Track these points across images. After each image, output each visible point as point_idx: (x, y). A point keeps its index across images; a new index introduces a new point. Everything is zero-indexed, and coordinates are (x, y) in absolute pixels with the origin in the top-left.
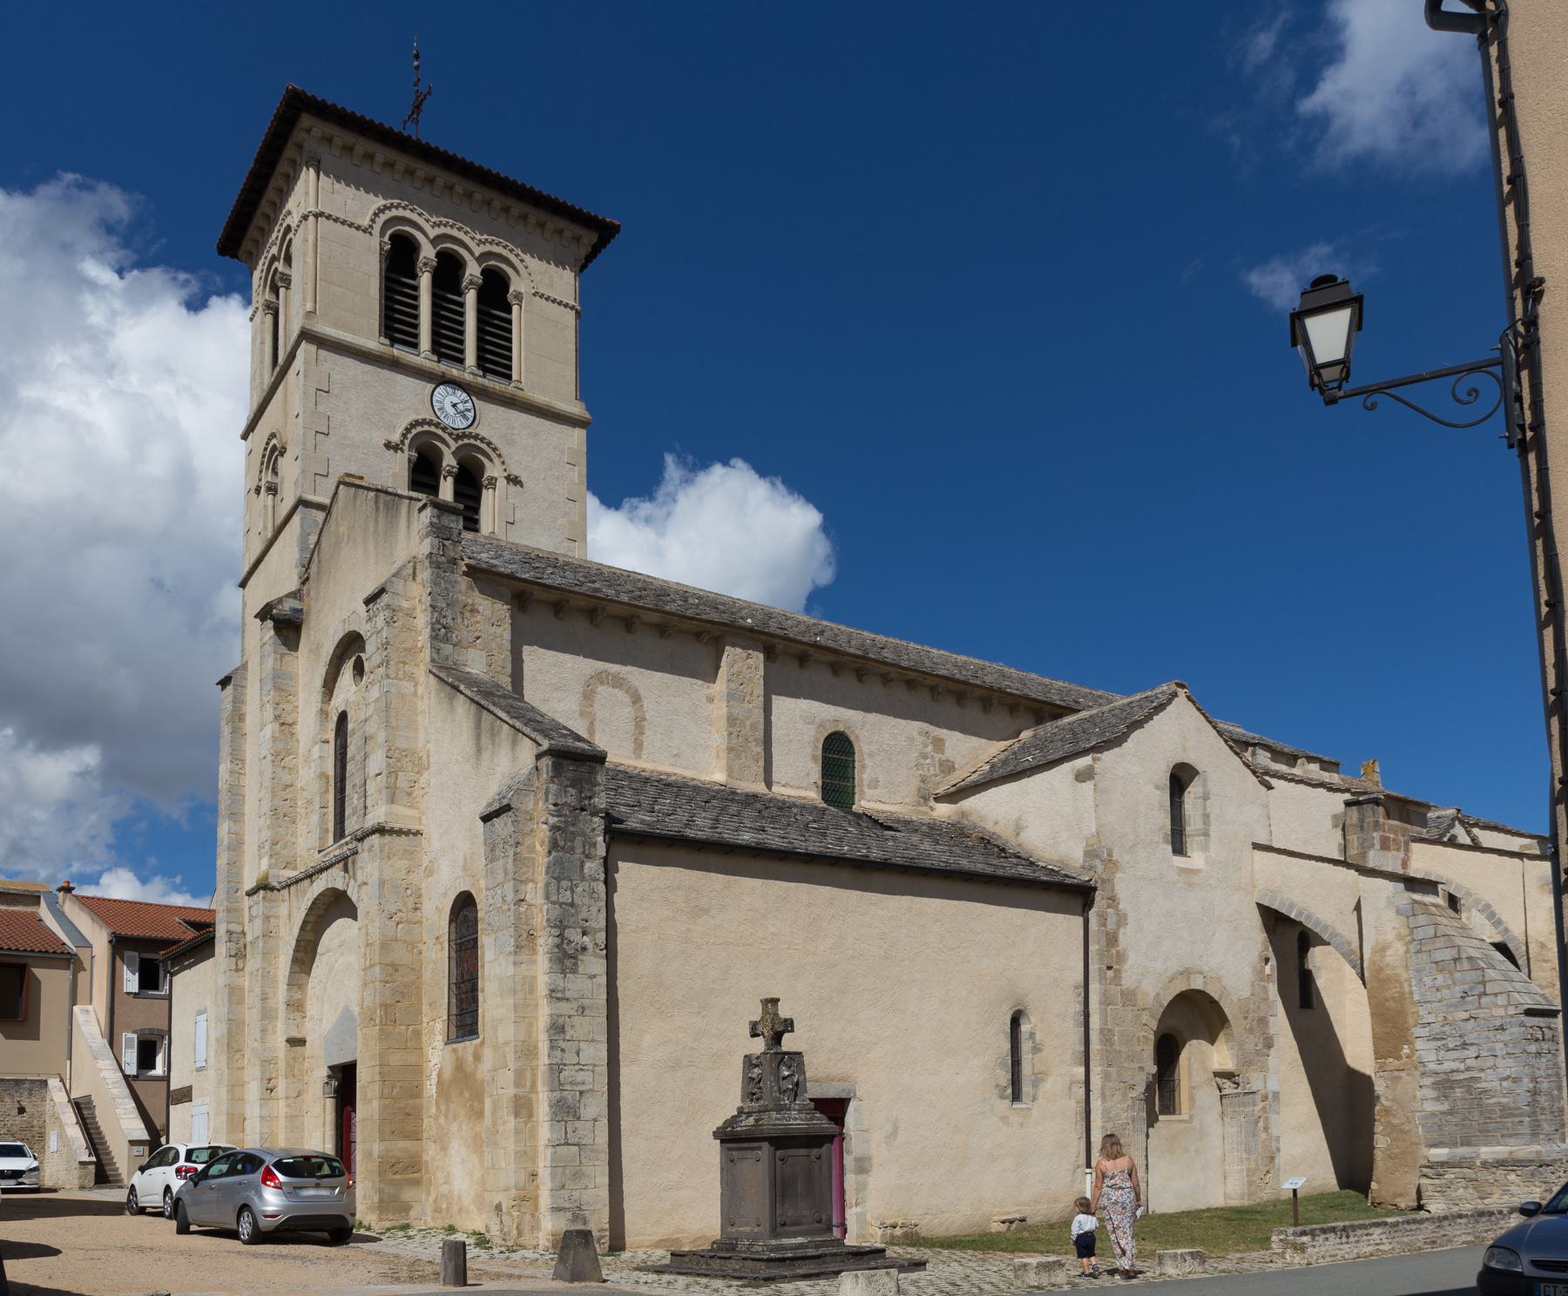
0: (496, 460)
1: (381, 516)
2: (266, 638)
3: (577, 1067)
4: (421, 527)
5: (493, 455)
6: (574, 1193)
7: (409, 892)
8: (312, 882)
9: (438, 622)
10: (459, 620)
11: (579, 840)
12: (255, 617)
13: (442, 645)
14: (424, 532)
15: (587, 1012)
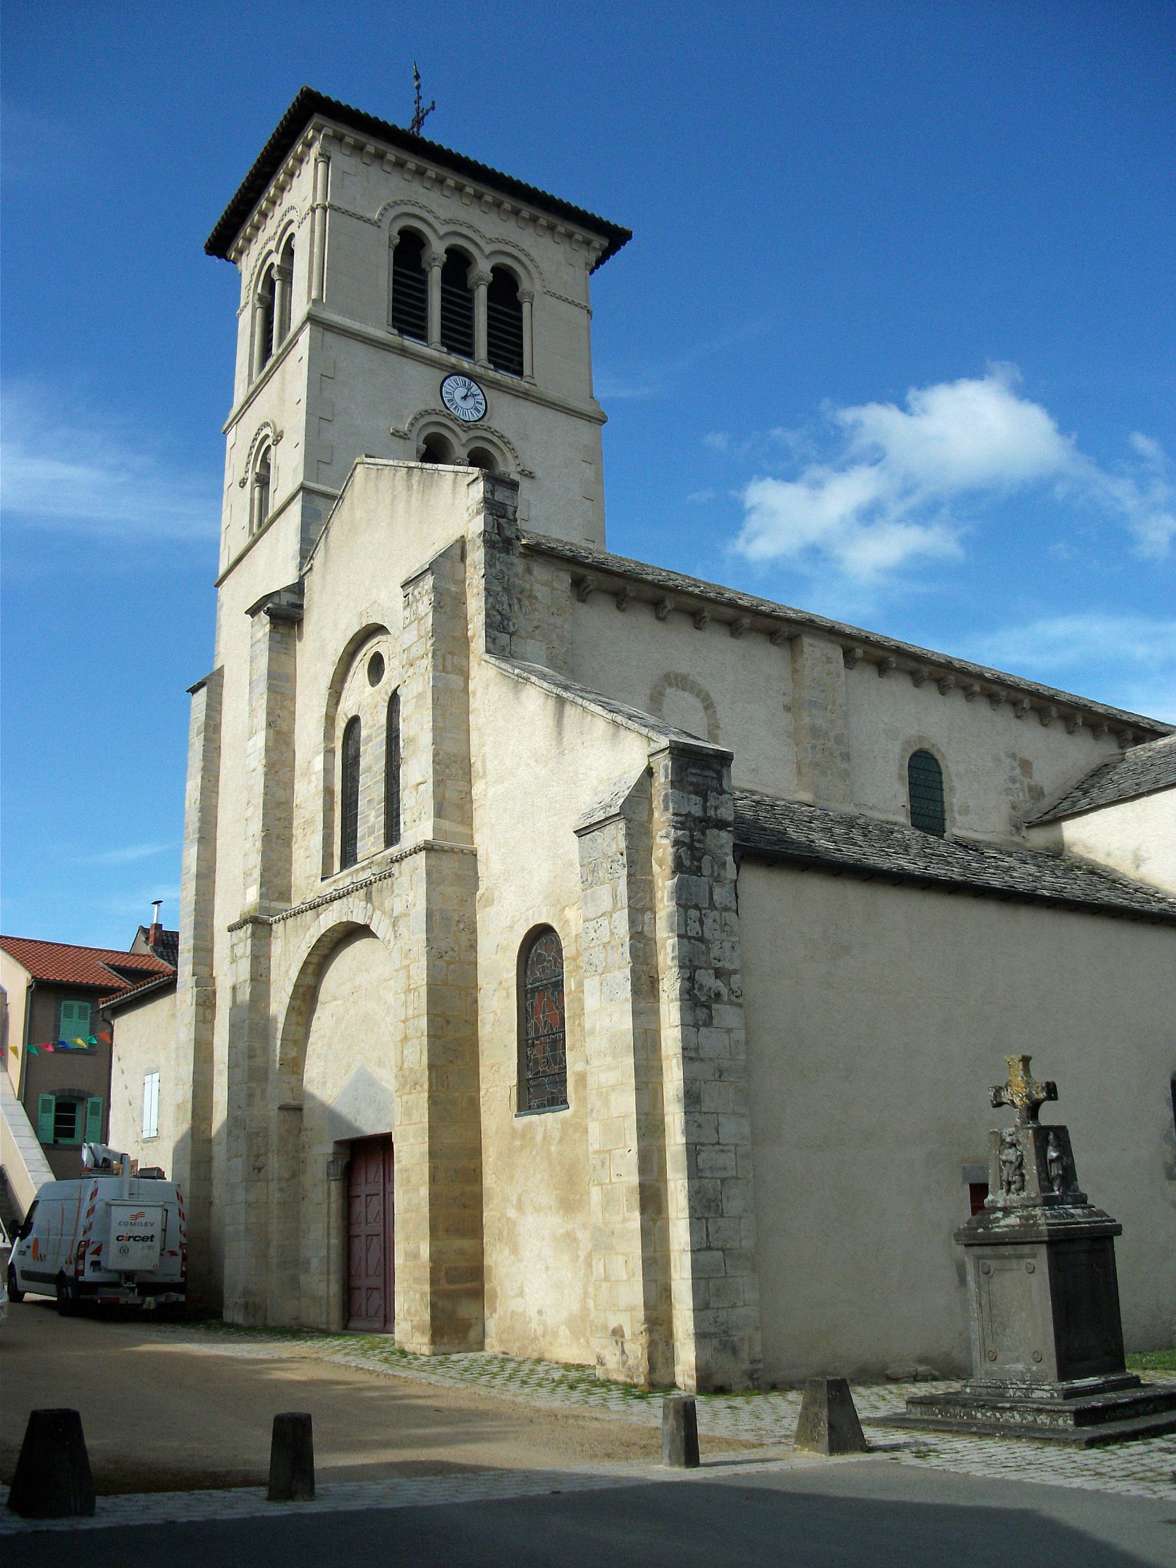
0: (509, 455)
1: (414, 499)
2: (260, 635)
3: (718, 1147)
4: (470, 503)
5: (505, 449)
6: (720, 1313)
7: (461, 926)
8: (318, 916)
9: (493, 607)
10: (516, 607)
11: (707, 859)
12: (246, 613)
13: (498, 634)
14: (474, 508)
15: (725, 1076)
